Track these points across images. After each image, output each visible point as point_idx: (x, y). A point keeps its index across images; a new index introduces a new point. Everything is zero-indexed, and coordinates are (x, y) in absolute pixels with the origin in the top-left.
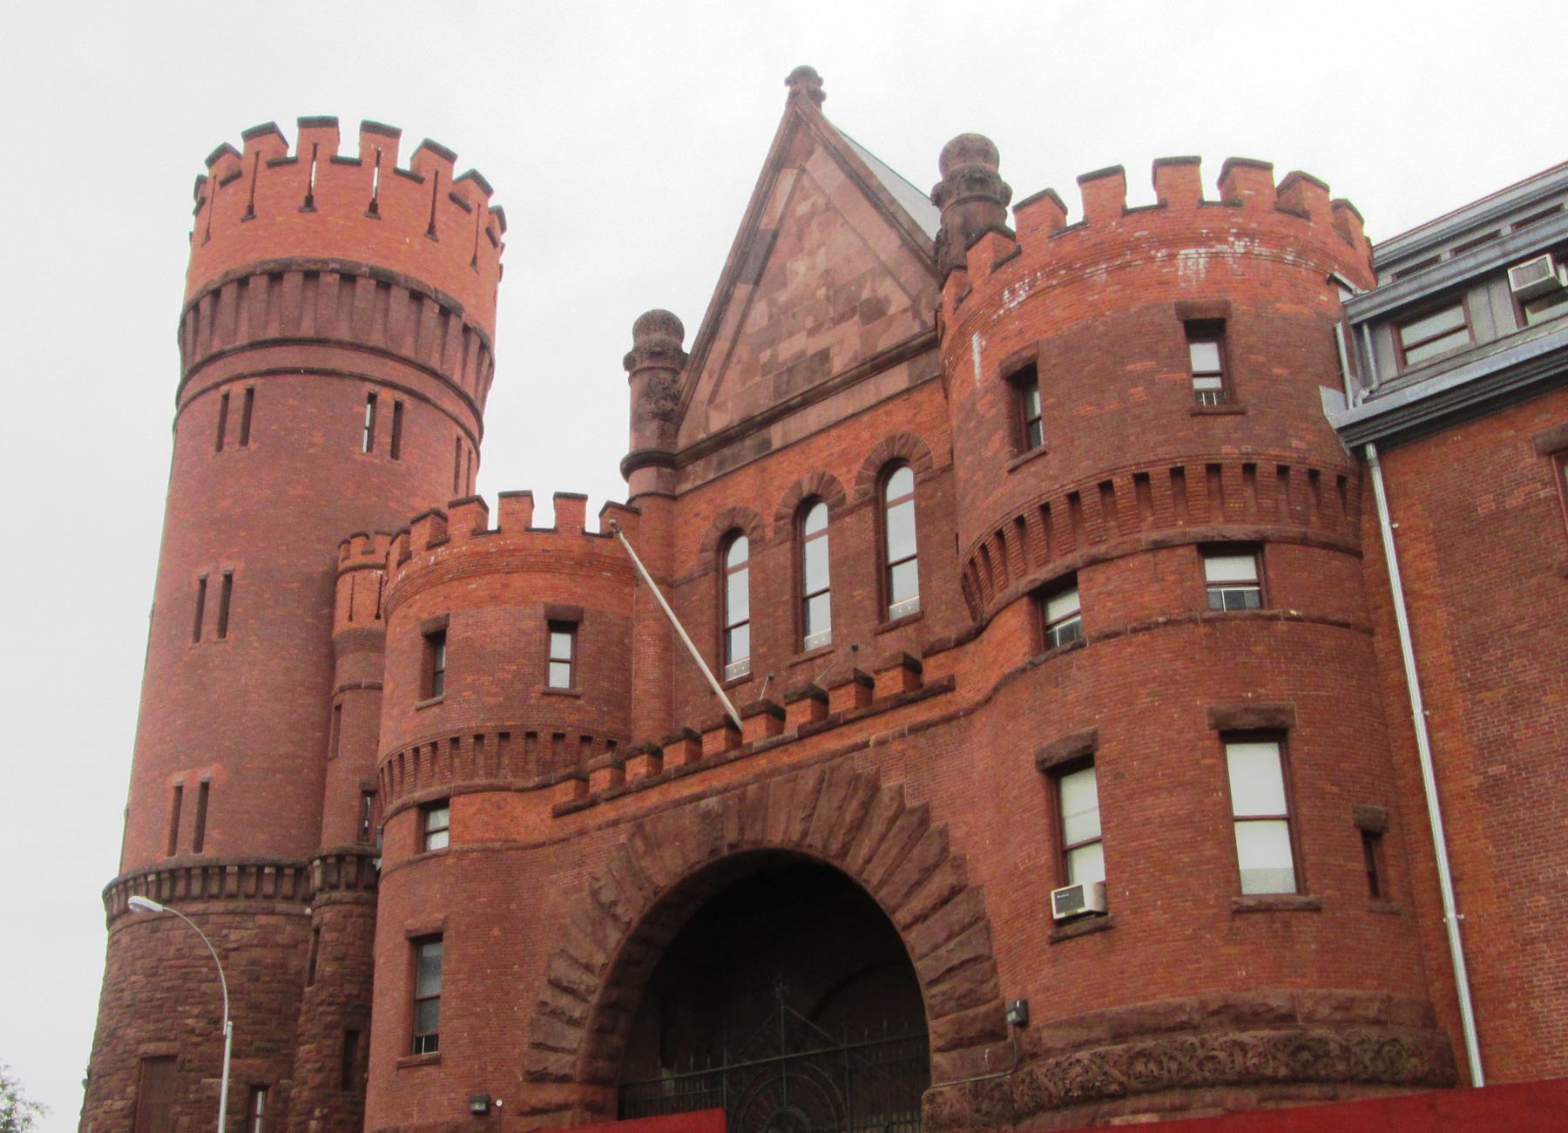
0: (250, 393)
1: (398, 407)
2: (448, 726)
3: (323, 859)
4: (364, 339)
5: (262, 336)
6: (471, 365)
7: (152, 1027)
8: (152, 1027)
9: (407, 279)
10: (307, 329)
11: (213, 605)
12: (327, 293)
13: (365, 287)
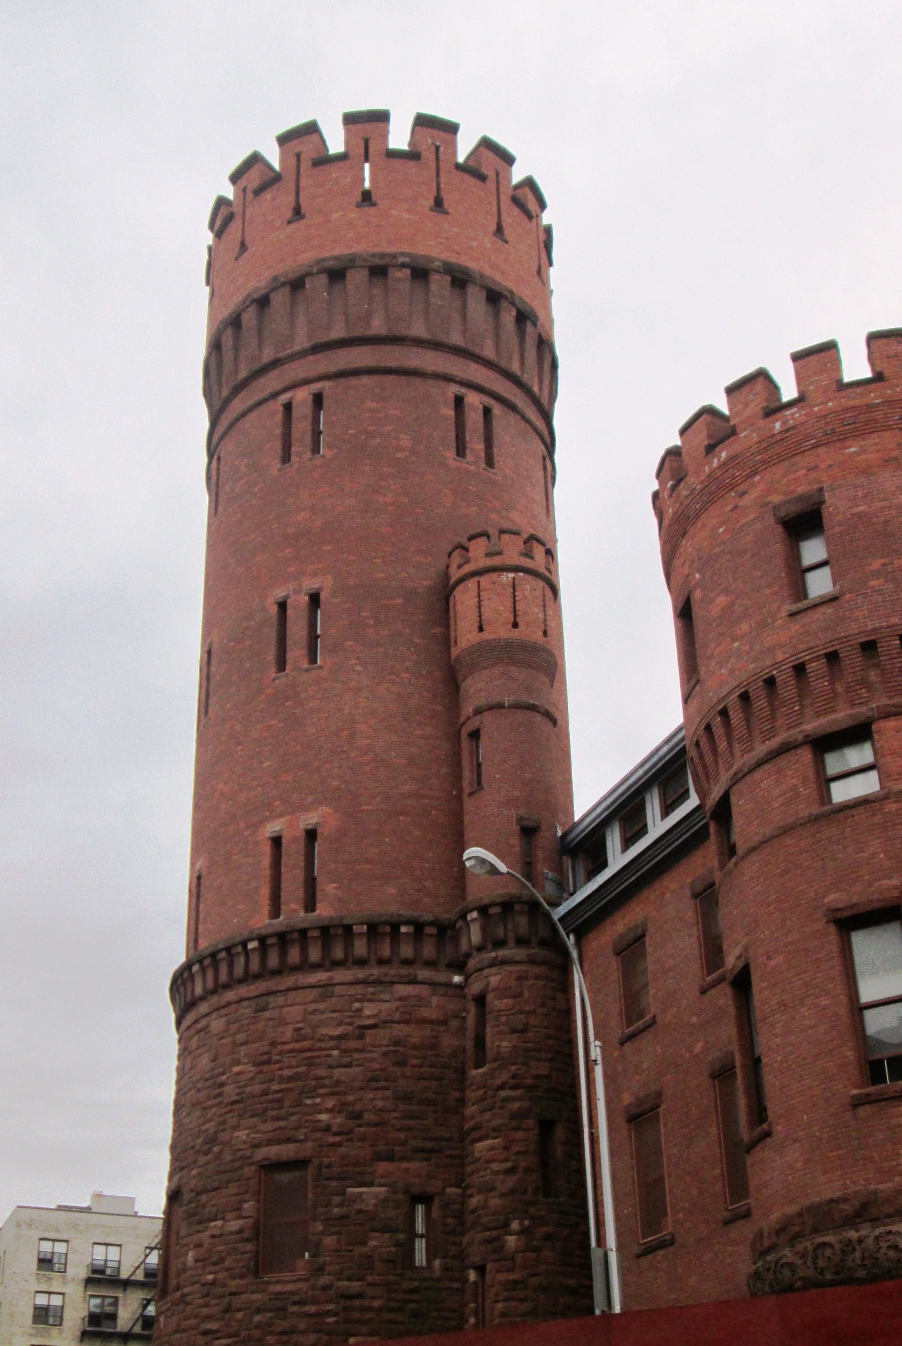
0: (318, 400)
1: (487, 411)
2: (854, 628)
3: (483, 910)
4: (442, 337)
5: (324, 338)
6: (546, 382)
7: (269, 1126)
8: (269, 1126)
9: (482, 276)
10: (378, 326)
11: (297, 629)
12: (375, 311)
13: (439, 284)
